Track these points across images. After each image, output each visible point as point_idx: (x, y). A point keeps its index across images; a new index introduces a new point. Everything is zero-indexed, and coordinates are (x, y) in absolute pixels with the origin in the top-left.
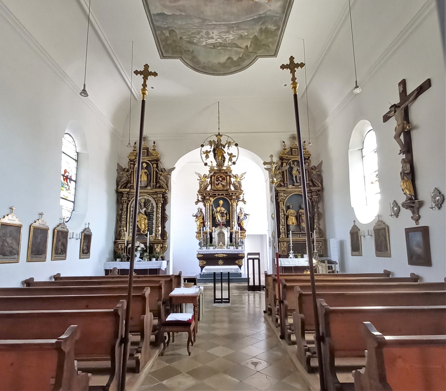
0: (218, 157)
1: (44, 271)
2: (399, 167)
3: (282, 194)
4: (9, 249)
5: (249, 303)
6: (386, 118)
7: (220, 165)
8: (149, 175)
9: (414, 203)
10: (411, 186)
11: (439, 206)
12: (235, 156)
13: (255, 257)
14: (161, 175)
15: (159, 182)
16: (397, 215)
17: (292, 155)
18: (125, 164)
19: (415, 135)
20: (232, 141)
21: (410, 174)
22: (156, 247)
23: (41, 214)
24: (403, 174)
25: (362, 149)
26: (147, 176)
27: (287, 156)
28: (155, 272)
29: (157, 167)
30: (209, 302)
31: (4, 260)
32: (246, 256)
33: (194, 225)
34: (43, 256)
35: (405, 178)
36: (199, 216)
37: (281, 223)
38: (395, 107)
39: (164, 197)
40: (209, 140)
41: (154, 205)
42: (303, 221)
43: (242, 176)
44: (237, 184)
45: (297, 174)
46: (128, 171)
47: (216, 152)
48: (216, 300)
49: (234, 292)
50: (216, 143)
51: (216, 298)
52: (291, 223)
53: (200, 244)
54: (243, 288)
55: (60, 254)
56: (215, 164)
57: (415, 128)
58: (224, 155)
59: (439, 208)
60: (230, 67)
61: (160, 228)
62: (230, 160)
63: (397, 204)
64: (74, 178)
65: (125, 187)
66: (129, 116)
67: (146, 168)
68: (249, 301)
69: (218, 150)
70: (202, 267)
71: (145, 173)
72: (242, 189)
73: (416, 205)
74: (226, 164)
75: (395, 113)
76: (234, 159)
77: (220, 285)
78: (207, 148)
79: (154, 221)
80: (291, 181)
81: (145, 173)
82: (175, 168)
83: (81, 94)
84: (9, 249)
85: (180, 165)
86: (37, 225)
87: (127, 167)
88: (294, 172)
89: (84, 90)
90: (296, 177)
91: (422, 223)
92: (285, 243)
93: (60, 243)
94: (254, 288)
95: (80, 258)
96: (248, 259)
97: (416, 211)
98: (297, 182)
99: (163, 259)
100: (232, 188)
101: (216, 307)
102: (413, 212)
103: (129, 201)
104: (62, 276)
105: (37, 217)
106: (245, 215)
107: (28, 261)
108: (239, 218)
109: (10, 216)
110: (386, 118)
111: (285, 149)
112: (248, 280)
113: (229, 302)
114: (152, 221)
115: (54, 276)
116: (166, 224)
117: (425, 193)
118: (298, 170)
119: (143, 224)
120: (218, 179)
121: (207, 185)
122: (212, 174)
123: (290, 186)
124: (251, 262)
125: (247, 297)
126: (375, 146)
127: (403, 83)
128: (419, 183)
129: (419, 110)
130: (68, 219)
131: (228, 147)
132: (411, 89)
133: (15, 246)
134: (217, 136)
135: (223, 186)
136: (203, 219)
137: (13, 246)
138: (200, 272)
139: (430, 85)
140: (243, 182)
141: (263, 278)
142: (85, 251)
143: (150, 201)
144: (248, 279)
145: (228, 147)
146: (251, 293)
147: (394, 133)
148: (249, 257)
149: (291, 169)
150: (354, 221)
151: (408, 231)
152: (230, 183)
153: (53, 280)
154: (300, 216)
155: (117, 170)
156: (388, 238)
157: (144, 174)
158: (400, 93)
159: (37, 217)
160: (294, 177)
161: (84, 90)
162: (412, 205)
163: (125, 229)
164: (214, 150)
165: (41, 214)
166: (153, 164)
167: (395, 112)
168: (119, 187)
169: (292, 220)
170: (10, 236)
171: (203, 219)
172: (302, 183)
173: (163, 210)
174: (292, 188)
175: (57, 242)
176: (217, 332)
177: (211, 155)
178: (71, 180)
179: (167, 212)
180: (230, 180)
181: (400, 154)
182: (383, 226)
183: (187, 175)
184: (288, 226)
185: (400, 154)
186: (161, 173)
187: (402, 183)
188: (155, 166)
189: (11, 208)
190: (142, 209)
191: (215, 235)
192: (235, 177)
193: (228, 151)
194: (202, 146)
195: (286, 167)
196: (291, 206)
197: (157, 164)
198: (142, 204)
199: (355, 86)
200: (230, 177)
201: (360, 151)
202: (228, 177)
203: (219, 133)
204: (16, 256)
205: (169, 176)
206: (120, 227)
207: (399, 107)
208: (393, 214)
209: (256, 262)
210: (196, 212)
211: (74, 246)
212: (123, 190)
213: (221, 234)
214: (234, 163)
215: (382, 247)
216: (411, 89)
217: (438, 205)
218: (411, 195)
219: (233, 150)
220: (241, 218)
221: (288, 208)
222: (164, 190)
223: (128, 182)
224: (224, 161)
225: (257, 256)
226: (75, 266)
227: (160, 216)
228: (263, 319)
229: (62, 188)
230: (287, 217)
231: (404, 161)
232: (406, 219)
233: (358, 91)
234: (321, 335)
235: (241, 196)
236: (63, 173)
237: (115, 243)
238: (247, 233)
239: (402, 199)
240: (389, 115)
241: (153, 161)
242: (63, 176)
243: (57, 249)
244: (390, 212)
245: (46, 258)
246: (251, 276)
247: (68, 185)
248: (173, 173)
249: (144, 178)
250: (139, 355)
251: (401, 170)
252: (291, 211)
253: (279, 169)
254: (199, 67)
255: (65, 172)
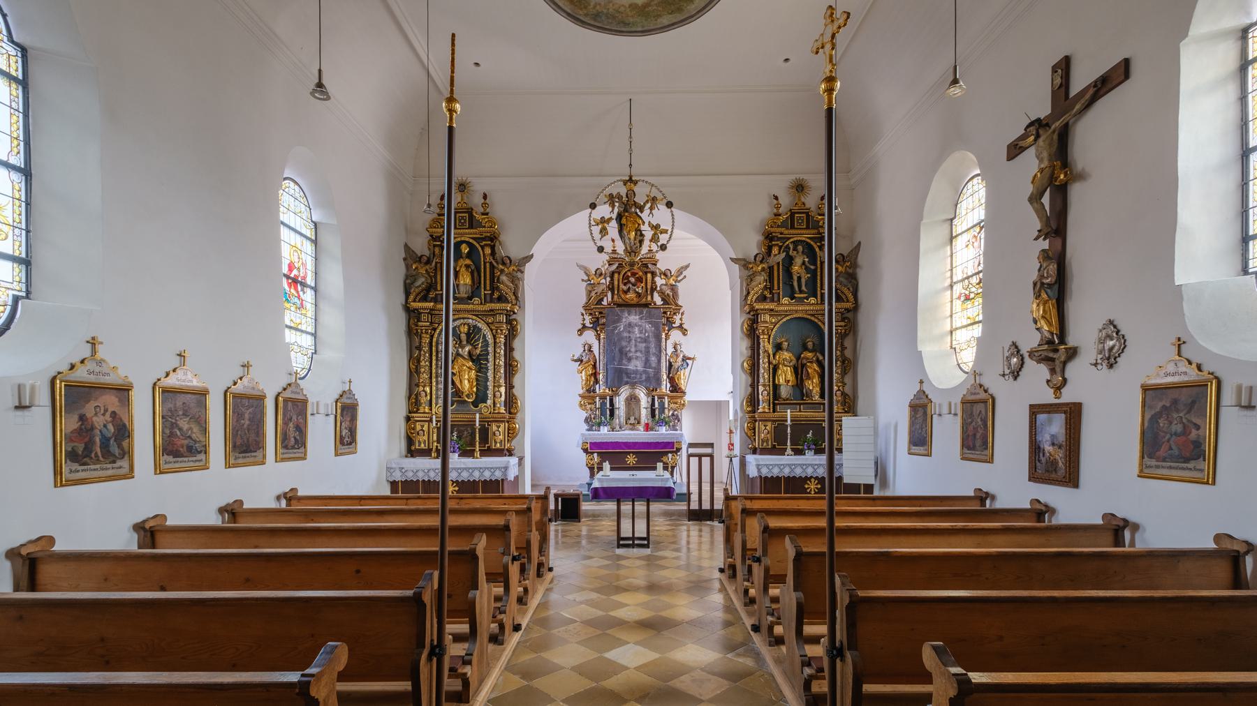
0: (629, 233)
1: (262, 485)
2: (1030, 268)
3: (767, 318)
4: (186, 442)
5: (689, 549)
6: (1015, 150)
7: (632, 251)
8: (475, 272)
9: (1056, 351)
10: (1054, 312)
11: (1111, 360)
12: (665, 231)
13: (703, 451)
14: (502, 271)
15: (498, 288)
16: (1016, 375)
17: (793, 227)
18: (421, 245)
19: (1077, 193)
20: (659, 196)
21: (1056, 287)
22: (494, 428)
23: (246, 366)
24: (1039, 287)
25: (952, 220)
26: (472, 273)
27: (783, 230)
28: (493, 486)
29: (493, 253)
30: (610, 543)
31: (177, 465)
32: (684, 447)
33: (576, 381)
34: (259, 454)
35: (1044, 296)
36: (586, 360)
37: (761, 380)
38: (1038, 125)
39: (509, 322)
40: (607, 192)
41: (489, 337)
42: (809, 377)
43: (680, 272)
44: (668, 291)
45: (803, 272)
46: (428, 262)
47: (624, 221)
48: (621, 542)
49: (660, 526)
50: (625, 199)
51: (623, 535)
52: (782, 381)
53: (587, 420)
54: (679, 514)
55: (293, 448)
56: (620, 248)
57: (1081, 177)
58: (642, 228)
59: (1111, 366)
60: (659, 16)
61: (503, 390)
62: (654, 239)
63: (1018, 351)
64: (310, 281)
65: (424, 299)
66: (427, 130)
67: (469, 255)
68: (688, 543)
69: (628, 212)
70: (592, 471)
71: (467, 266)
72: (680, 303)
73: (1061, 355)
74: (645, 250)
75: (1035, 140)
76: (663, 238)
77: (630, 507)
78: (604, 211)
79: (490, 374)
80: (788, 288)
81: (467, 266)
82: (532, 256)
83: (312, 94)
84: (186, 442)
85: (544, 248)
86: (239, 388)
87: (427, 253)
88: (796, 268)
89: (320, 85)
90: (799, 278)
91: (1068, 396)
92: (769, 424)
93: (291, 425)
94: (699, 516)
95: (336, 455)
96: (690, 456)
97: (1058, 369)
98: (801, 292)
99: (510, 453)
100: (658, 300)
101: (620, 558)
102: (1053, 371)
103: (435, 329)
104: (300, 494)
105: (239, 372)
106: (685, 359)
107: (228, 465)
108: (671, 365)
109: (180, 373)
110: (1015, 150)
111: (777, 215)
112: (686, 497)
113: (647, 546)
114: (486, 374)
115: (285, 494)
116: (516, 381)
117: (1084, 330)
118: (804, 263)
119: (467, 383)
120: (626, 280)
121: (604, 294)
122: (614, 267)
123: (785, 300)
124: (694, 461)
125: (685, 534)
126: (980, 214)
127: (1064, 67)
128: (1074, 307)
129: (1094, 137)
130: (305, 372)
131: (651, 208)
132: (1081, 80)
133: (196, 433)
134: (625, 183)
135: (639, 295)
136: (594, 366)
137: (194, 436)
138: (588, 480)
139: (1127, 75)
140: (681, 287)
141: (719, 495)
142: (346, 440)
143: (480, 330)
144: (689, 494)
145: (651, 208)
146: (694, 527)
147: (1030, 189)
148: (691, 451)
149: (789, 260)
150: (921, 382)
151: (1035, 410)
152: (653, 289)
153: (283, 504)
154: (803, 366)
155: (405, 259)
156: (990, 423)
157: (463, 269)
158: (1053, 92)
159: (239, 372)
160: (795, 278)
161: (320, 85)
162: (1051, 355)
163: (428, 389)
164: (619, 217)
165: (246, 366)
166: (483, 248)
167: (1038, 136)
168: (412, 297)
169: (786, 376)
170: (185, 415)
171: (594, 366)
172: (813, 286)
173: (509, 349)
174: (790, 304)
175: (285, 424)
176: (621, 613)
177: (613, 228)
178: (304, 285)
179: (516, 355)
180: (653, 282)
181: (1036, 239)
182: (982, 395)
183: (560, 260)
184: (776, 387)
185: (1036, 239)
186: (501, 267)
187: (1035, 306)
188: (488, 251)
189: (180, 355)
190: (463, 347)
191: (620, 402)
192: (665, 275)
193: (650, 218)
194: (593, 206)
195: (778, 257)
196: (785, 344)
197: (493, 248)
198: (463, 337)
199: (951, 78)
200: (653, 274)
201: (947, 225)
202: (649, 275)
203: (631, 177)
204: (202, 456)
205: (519, 274)
206: (418, 385)
207: (1048, 125)
208: (1007, 371)
209: (706, 461)
210: (578, 352)
211: (321, 430)
212: (420, 304)
213: (632, 400)
214: (663, 248)
215: (977, 441)
216: (1080, 82)
217: (1108, 359)
218: (1052, 334)
219: (661, 215)
220: (676, 365)
221: (778, 347)
222: (509, 307)
223: (431, 287)
224: (641, 242)
225: (708, 451)
226: (326, 473)
227: (502, 363)
228: (717, 585)
229: (287, 305)
230: (775, 369)
231: (1045, 256)
232: (1036, 383)
233: (955, 91)
234: (837, 644)
235: (677, 318)
236: (285, 270)
237: (408, 419)
238: (687, 398)
239: (1030, 340)
240: (1022, 144)
241: (484, 239)
242: (288, 277)
243: (285, 437)
244: (1000, 367)
245: (264, 457)
246: (694, 488)
247: (299, 297)
248: (529, 268)
249: (466, 279)
250: (467, 670)
251: (1035, 276)
252: (786, 355)
253: (761, 262)
254: (586, 15)
255: (291, 267)
